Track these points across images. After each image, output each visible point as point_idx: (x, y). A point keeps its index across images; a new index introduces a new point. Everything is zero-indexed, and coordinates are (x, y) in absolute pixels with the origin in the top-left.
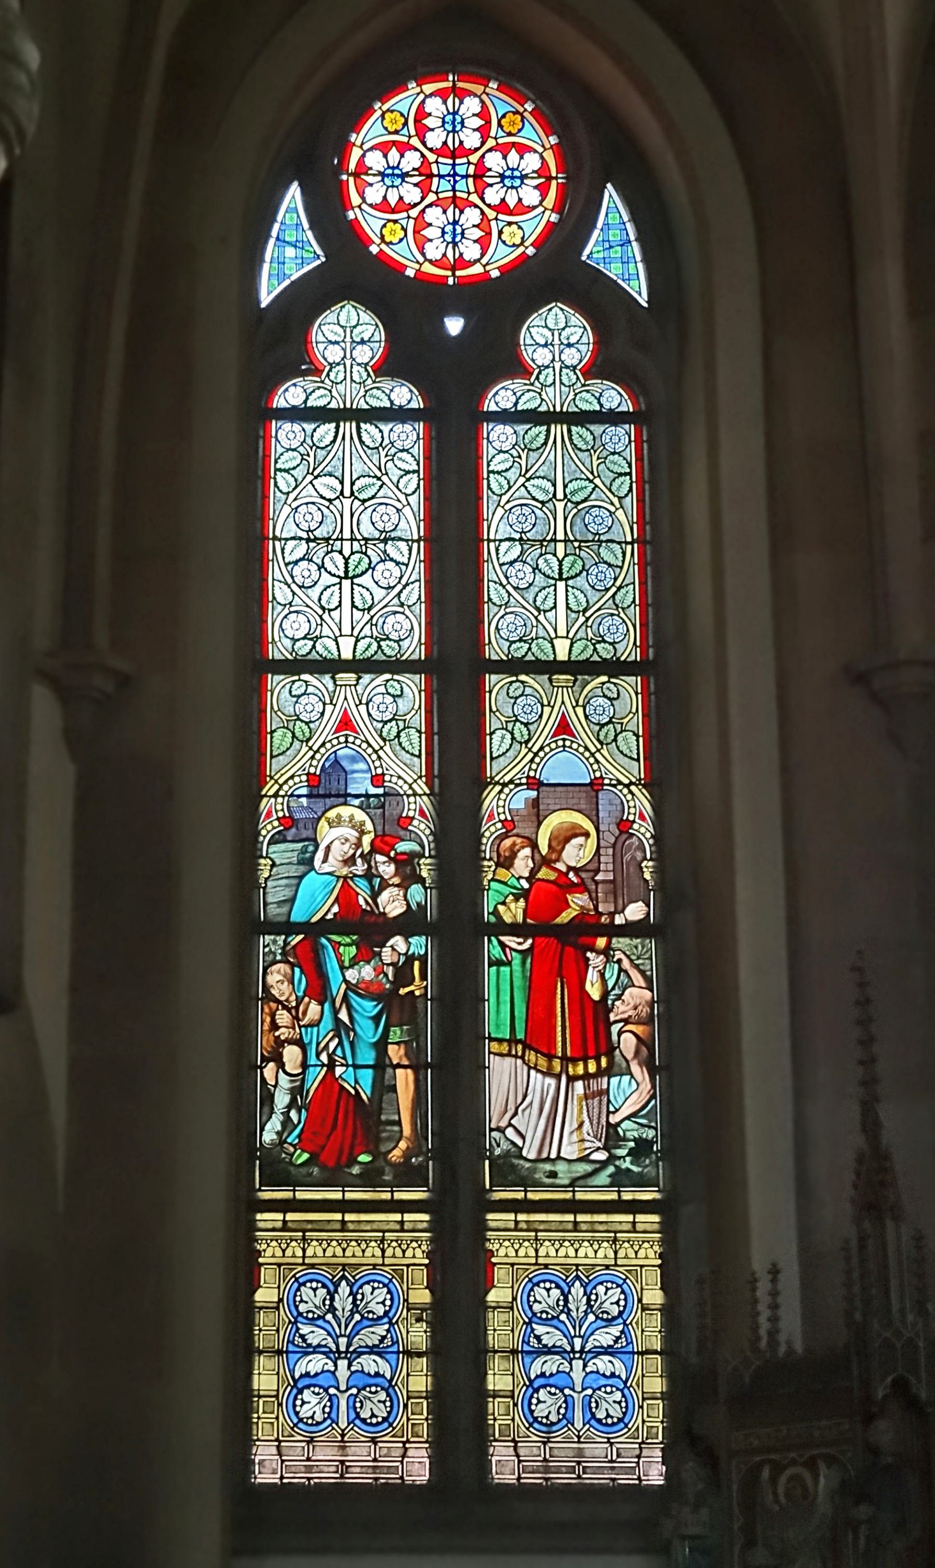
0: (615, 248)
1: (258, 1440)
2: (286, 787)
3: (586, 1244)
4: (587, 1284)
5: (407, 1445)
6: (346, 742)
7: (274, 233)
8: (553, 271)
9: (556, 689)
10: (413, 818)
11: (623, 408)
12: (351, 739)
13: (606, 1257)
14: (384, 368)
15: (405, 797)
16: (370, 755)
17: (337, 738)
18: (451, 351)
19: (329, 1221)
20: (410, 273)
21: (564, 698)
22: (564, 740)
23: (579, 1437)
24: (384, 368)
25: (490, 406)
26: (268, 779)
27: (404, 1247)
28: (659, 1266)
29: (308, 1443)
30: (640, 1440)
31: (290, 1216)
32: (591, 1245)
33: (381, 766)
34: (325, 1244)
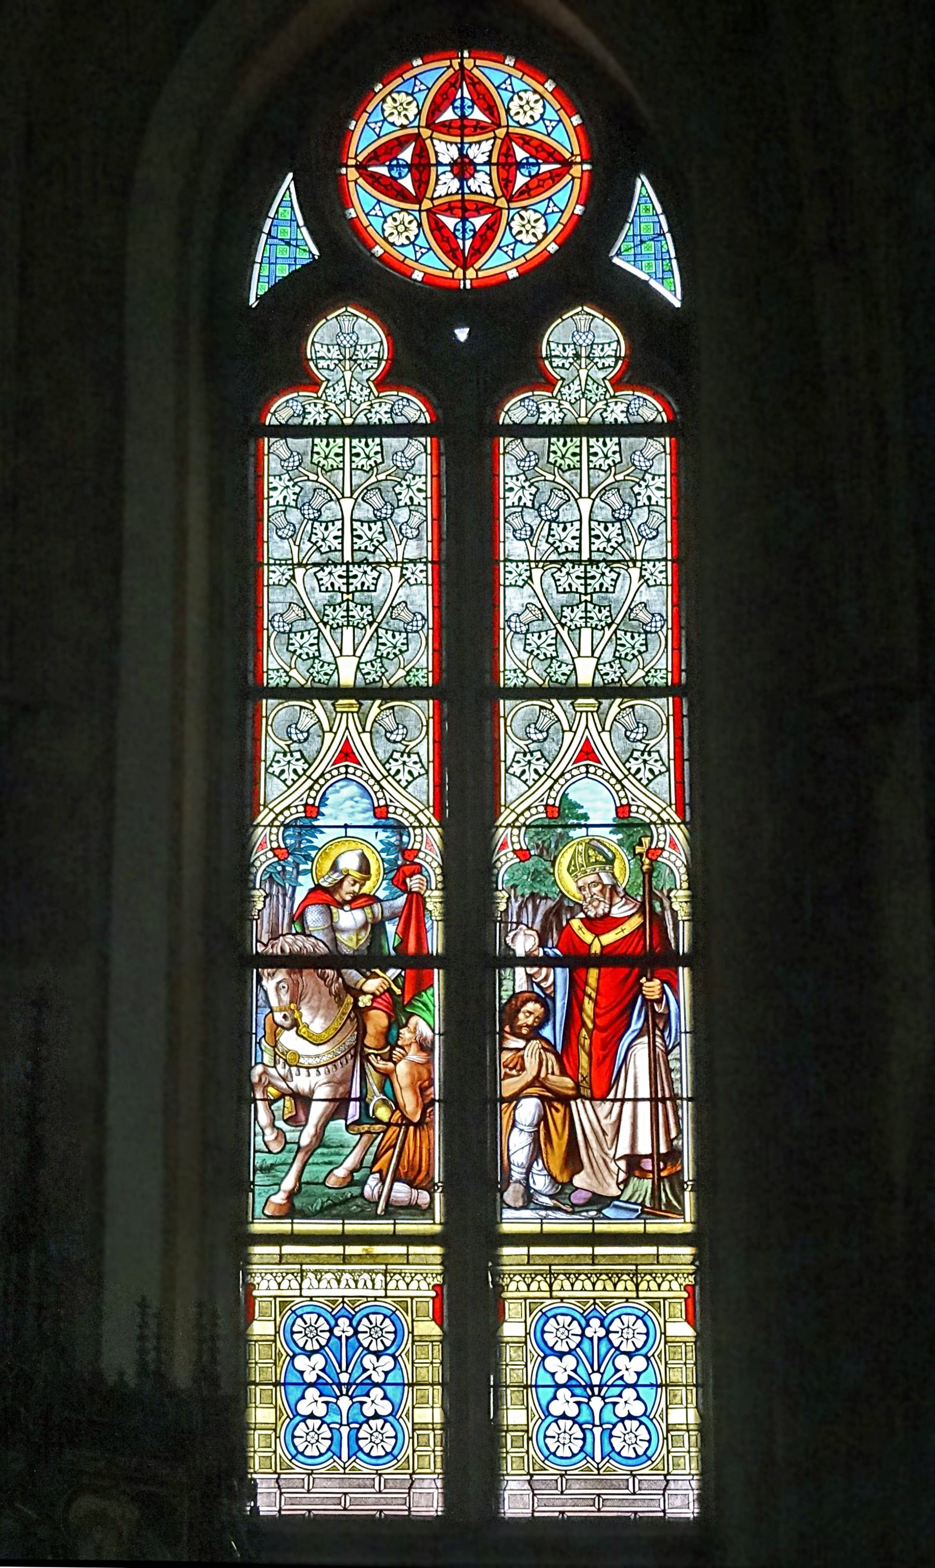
0: (647, 252)
1: (508, 1474)
2: (281, 818)
3: (625, 1277)
4: (354, 1316)
5: (669, 1477)
6: (587, 772)
7: (266, 230)
8: (579, 271)
9: (339, 715)
10: (663, 849)
11: (422, 421)
12: (592, 770)
13: (626, 1289)
14: (629, 377)
15: (411, 829)
16: (371, 787)
17: (337, 769)
18: (466, 360)
19: (578, 1256)
20: (513, 274)
21: (346, 724)
22: (587, 766)
23: (598, 1469)
24: (629, 377)
25: (503, 419)
26: (503, 809)
27: (659, 1280)
28: (433, 1298)
29: (562, 1476)
30: (411, 1471)
31: (535, 1250)
32: (654, 1278)
33: (626, 797)
34: (594, 1279)
